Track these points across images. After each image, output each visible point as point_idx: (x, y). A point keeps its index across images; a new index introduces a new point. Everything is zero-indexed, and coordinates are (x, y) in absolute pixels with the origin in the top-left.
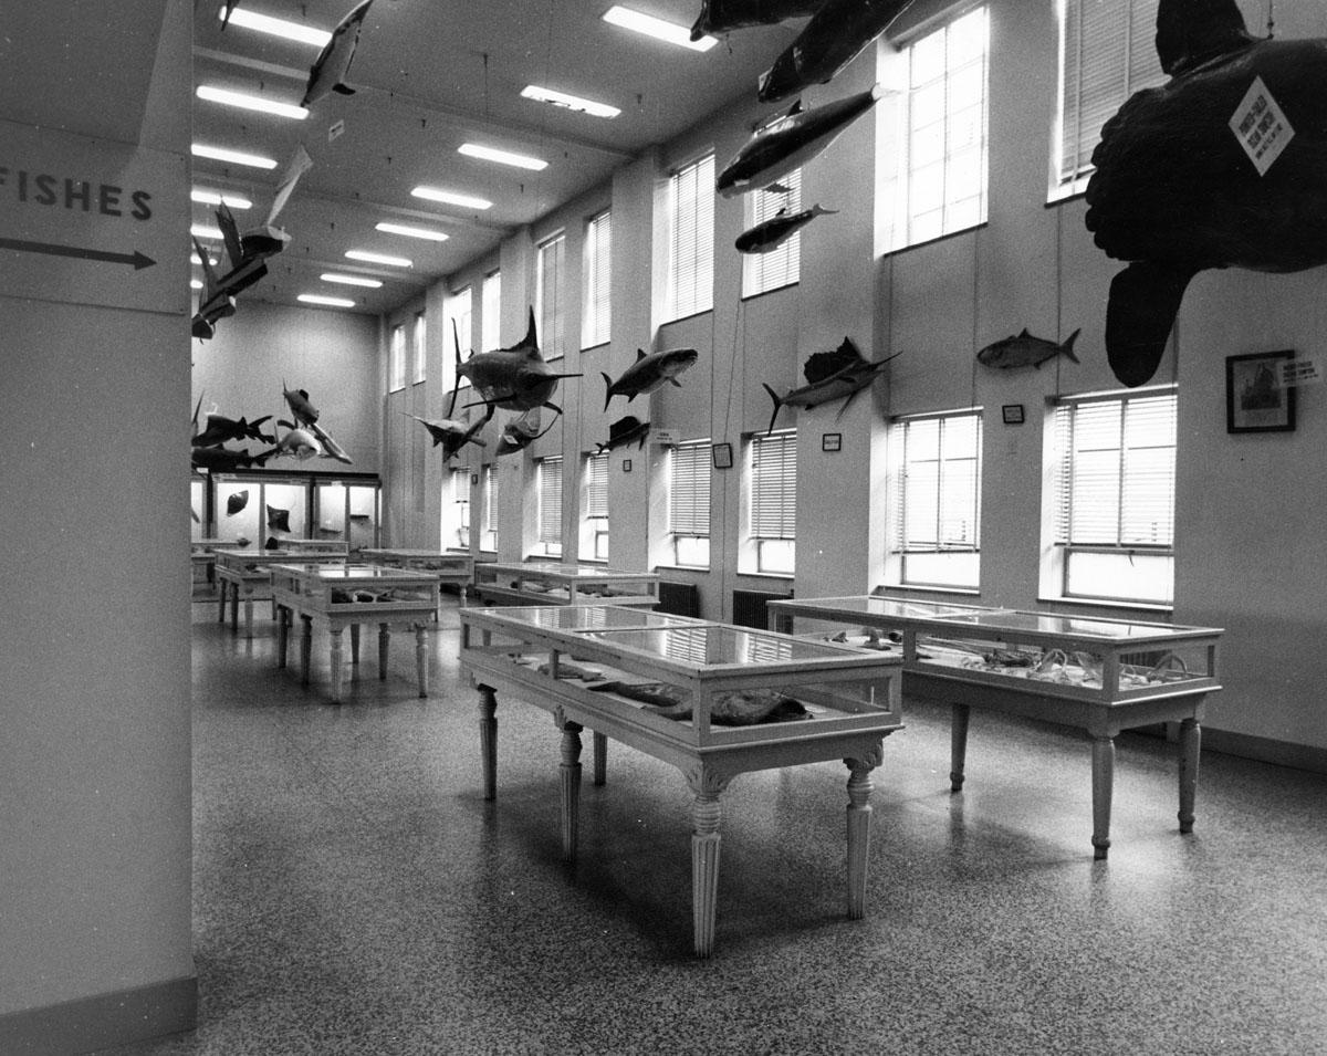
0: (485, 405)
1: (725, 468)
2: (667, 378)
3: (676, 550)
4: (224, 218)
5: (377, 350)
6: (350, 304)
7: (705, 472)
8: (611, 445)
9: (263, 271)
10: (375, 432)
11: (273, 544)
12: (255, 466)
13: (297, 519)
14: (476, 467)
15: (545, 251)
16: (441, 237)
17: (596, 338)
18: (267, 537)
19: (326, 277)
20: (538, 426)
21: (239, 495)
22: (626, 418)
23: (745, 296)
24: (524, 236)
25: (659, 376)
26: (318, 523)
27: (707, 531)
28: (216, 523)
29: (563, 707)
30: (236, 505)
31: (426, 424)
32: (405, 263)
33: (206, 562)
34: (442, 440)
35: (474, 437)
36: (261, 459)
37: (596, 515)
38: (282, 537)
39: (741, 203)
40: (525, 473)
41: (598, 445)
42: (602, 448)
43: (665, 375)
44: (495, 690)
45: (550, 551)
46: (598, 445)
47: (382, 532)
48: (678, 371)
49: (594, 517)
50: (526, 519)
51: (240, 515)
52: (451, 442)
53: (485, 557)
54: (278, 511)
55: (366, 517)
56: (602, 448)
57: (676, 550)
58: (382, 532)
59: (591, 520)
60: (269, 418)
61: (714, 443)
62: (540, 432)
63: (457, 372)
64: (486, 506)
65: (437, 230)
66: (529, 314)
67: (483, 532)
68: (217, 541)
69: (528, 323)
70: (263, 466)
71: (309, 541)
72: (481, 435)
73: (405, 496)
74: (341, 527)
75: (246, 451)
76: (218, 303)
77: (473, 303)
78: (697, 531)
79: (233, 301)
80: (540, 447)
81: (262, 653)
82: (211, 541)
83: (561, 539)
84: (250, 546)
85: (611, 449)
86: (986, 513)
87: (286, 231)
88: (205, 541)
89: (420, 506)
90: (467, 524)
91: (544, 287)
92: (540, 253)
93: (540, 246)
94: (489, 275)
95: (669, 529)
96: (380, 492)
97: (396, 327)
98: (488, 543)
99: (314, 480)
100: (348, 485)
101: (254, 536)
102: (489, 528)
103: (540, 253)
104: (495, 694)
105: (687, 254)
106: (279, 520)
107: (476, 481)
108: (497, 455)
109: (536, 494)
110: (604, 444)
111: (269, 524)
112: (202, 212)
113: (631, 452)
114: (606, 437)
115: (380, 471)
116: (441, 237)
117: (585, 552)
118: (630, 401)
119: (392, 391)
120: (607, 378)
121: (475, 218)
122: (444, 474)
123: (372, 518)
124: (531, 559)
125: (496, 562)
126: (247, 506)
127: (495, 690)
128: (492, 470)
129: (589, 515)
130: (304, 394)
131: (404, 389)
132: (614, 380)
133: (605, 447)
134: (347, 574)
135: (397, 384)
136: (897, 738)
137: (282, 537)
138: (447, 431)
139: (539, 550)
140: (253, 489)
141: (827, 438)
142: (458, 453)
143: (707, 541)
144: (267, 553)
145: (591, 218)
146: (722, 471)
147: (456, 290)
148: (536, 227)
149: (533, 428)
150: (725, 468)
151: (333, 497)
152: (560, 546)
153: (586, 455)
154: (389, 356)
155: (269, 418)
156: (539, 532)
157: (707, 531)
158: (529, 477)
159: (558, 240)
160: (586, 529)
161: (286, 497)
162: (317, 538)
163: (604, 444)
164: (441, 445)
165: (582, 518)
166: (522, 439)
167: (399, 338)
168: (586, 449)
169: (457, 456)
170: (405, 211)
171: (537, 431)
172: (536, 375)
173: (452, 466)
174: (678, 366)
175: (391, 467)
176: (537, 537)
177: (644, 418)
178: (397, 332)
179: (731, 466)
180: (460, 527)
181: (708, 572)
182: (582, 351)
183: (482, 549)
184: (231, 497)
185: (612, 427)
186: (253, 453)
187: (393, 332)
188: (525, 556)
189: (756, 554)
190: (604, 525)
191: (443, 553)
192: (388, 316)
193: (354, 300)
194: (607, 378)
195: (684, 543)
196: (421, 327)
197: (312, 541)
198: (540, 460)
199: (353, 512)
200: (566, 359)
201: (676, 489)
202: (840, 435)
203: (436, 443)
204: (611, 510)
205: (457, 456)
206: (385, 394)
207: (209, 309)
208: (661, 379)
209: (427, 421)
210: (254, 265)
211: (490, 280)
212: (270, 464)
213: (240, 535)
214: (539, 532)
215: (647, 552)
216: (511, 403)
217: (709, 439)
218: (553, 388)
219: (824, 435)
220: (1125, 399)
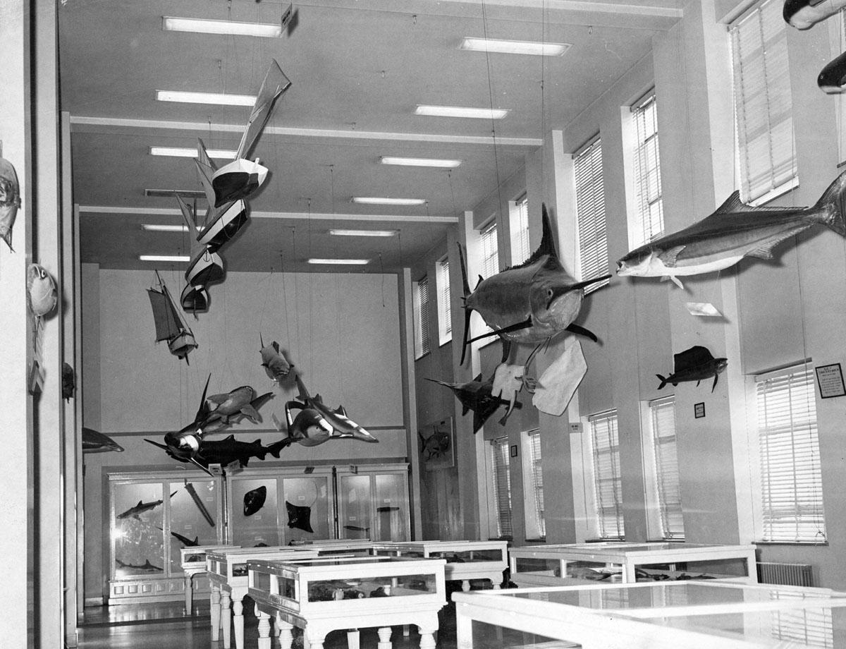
27: (402, 425)
31: (452, 388)
33: (288, 410)
41: (660, 377)
44: (141, 502)
46: (660, 377)
86: (341, 632)
104: (143, 503)
108: (312, 531)
110: (667, 377)
114: (669, 369)
127: (141, 502)
133: (669, 380)
142: (669, 376)
163: (667, 377)
164: (471, 413)
169: (670, 374)
189: (68, 632)
205: (670, 374)
209: (454, 384)
219: (695, 405)
220: (790, 388)
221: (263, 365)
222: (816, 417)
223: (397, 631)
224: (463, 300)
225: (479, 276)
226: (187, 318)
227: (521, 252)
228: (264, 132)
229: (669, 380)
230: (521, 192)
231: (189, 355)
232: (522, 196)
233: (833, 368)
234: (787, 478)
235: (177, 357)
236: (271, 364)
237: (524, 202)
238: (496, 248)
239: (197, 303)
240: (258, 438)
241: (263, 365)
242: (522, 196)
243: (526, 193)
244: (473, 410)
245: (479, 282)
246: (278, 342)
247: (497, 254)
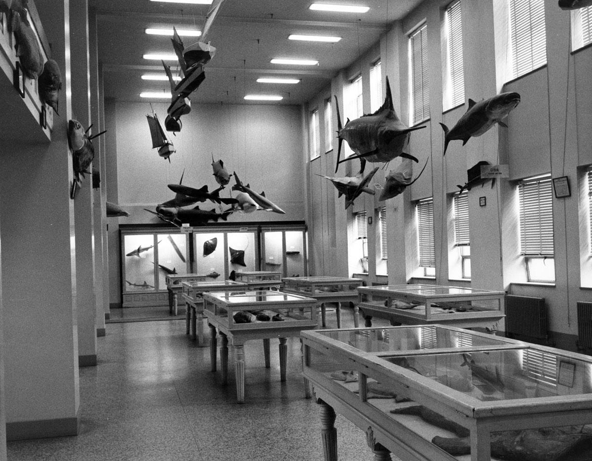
0: (359, 159)
1: (564, 197)
2: (494, 121)
3: (527, 269)
4: (176, 44)
5: (300, 132)
6: (279, 98)
7: (547, 203)
8: (469, 186)
9: (202, 77)
10: (301, 193)
11: (233, 276)
12: (220, 221)
13: (250, 257)
14: (370, 212)
15: (413, 39)
16: (336, 39)
17: (455, 102)
18: (230, 271)
19: (260, 80)
20: (411, 175)
21: (211, 242)
23: (574, 49)
24: (397, 30)
25: (487, 120)
26: (264, 259)
27: (552, 252)
28: (196, 262)
29: (373, 429)
30: (209, 249)
31: (332, 181)
32: (313, 62)
34: (344, 193)
35: (365, 188)
36: (224, 216)
37: (461, 243)
38: (240, 270)
40: (405, 213)
41: (459, 186)
42: (462, 188)
43: (493, 118)
45: (428, 273)
46: (459, 186)
47: (309, 266)
48: (504, 113)
49: (459, 245)
50: (408, 248)
51: (211, 256)
52: (350, 192)
53: (380, 281)
54: (237, 251)
55: (298, 253)
56: (462, 188)
57: (527, 269)
58: (309, 266)
59: (457, 247)
61: (554, 177)
62: (412, 180)
63: (339, 137)
64: (379, 240)
65: (332, 35)
66: (385, 84)
67: (378, 260)
68: (198, 275)
70: (226, 220)
71: (258, 272)
72: (371, 186)
73: (323, 236)
74: (281, 262)
75: (214, 210)
76: (178, 104)
77: (363, 88)
78: (543, 252)
79: (188, 102)
80: (417, 191)
81: (161, 371)
82: (194, 275)
83: (434, 264)
84: (219, 277)
85: (469, 190)
87: (212, 45)
88: (190, 275)
89: (333, 243)
90: (366, 255)
91: (414, 65)
92: (410, 41)
93: (409, 36)
94: (374, 64)
95: (520, 251)
96: (307, 234)
97: (313, 112)
98: (382, 270)
99: (259, 228)
100: (284, 231)
101: (221, 271)
102: (382, 257)
103: (410, 41)
105: (524, 23)
106: (238, 258)
107: (372, 222)
109: (415, 230)
110: (463, 185)
111: (231, 261)
112: (158, 44)
113: (485, 191)
114: (464, 180)
115: (306, 218)
116: (336, 39)
117: (455, 273)
118: (464, 144)
119: (312, 159)
120: (444, 127)
121: (358, 21)
122: (348, 219)
123: (302, 253)
124: (414, 281)
125: (386, 284)
126: (216, 249)
128: (382, 212)
129: (455, 243)
130: (221, 163)
131: (320, 157)
132: (450, 128)
133: (465, 187)
135: (315, 154)
137: (240, 270)
138: (346, 185)
139: (419, 273)
140: (220, 236)
143: (553, 260)
144: (230, 282)
145: (446, 8)
146: (562, 200)
147: (352, 78)
148: (405, 21)
149: (408, 177)
150: (564, 197)
151: (273, 239)
152: (434, 269)
153: (451, 196)
154: (309, 132)
156: (419, 258)
157: (552, 252)
158: (409, 215)
159: (421, 28)
160: (454, 255)
161: (242, 241)
162: (264, 270)
163: (463, 185)
164: (344, 196)
165: (450, 246)
166: (395, 187)
167: (315, 120)
168: (451, 191)
170: (304, 23)
171: (410, 179)
172: (392, 132)
173: (355, 211)
174: (503, 109)
175: (313, 216)
176: (417, 263)
177: (493, 159)
178: (314, 115)
179: (570, 195)
180: (362, 257)
181: (554, 287)
182: (444, 113)
183: (377, 274)
184: (206, 243)
185: (469, 171)
186: (218, 212)
187: (311, 116)
188: (408, 278)
190: (467, 251)
191: (350, 278)
192: (307, 104)
193: (282, 95)
194: (444, 127)
195: (535, 263)
196: (329, 111)
197: (262, 272)
198: (417, 202)
199: (288, 250)
200: (432, 120)
201: (524, 218)
203: (340, 195)
204: (472, 238)
206: (307, 162)
207: (174, 109)
208: (488, 123)
209: (333, 178)
210: (197, 73)
211: (375, 68)
212: (230, 219)
213: (212, 270)
214: (419, 258)
215: (502, 275)
216: (375, 156)
217: (550, 175)
218: (406, 140)
219: (480, 198)
221: (214, 174)
222: (553, 251)
223: (307, 276)
224: (337, 133)
225: (348, 119)
226: (169, 135)
227: (377, 103)
228: (128, 288)
229: (465, 187)
230: (378, 57)
231: (170, 156)
232: (378, 60)
233: (564, 179)
234: (519, 27)
235: (163, 158)
236: (219, 174)
237: (379, 64)
238: (362, 93)
239: (173, 126)
240: (214, 208)
241: (214, 174)
242: (378, 60)
243: (380, 59)
244: (346, 194)
245: (348, 122)
246: (223, 161)
247: (362, 95)
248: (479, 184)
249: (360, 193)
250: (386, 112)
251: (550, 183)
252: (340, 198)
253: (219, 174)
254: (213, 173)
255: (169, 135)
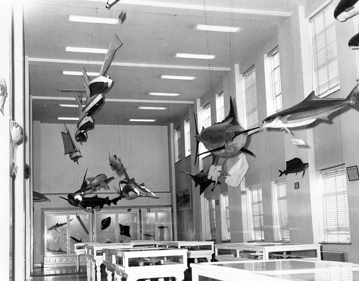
22: (300, 159)
31: (191, 175)
39: (163, 230)
41: (280, 171)
60: (60, 197)
69: (349, 245)
110: (283, 171)
114: (284, 168)
134: (156, 215)
136: (64, 258)
141: (296, 184)
155: (60, 197)
163: (283, 171)
164: (199, 186)
202: (357, 166)
207: (76, 137)
209: (192, 174)
219: (295, 183)
221: (110, 165)
224: (195, 137)
225: (203, 127)
226: (78, 144)
229: (284, 172)
231: (78, 160)
232: (222, 92)
237: (222, 95)
241: (110, 165)
242: (222, 92)
244: (200, 185)
248: (294, 172)
249: (210, 183)
250: (231, 120)
251: (345, 173)
252: (196, 188)
253: (113, 164)
254: (109, 164)
255: (78, 144)
